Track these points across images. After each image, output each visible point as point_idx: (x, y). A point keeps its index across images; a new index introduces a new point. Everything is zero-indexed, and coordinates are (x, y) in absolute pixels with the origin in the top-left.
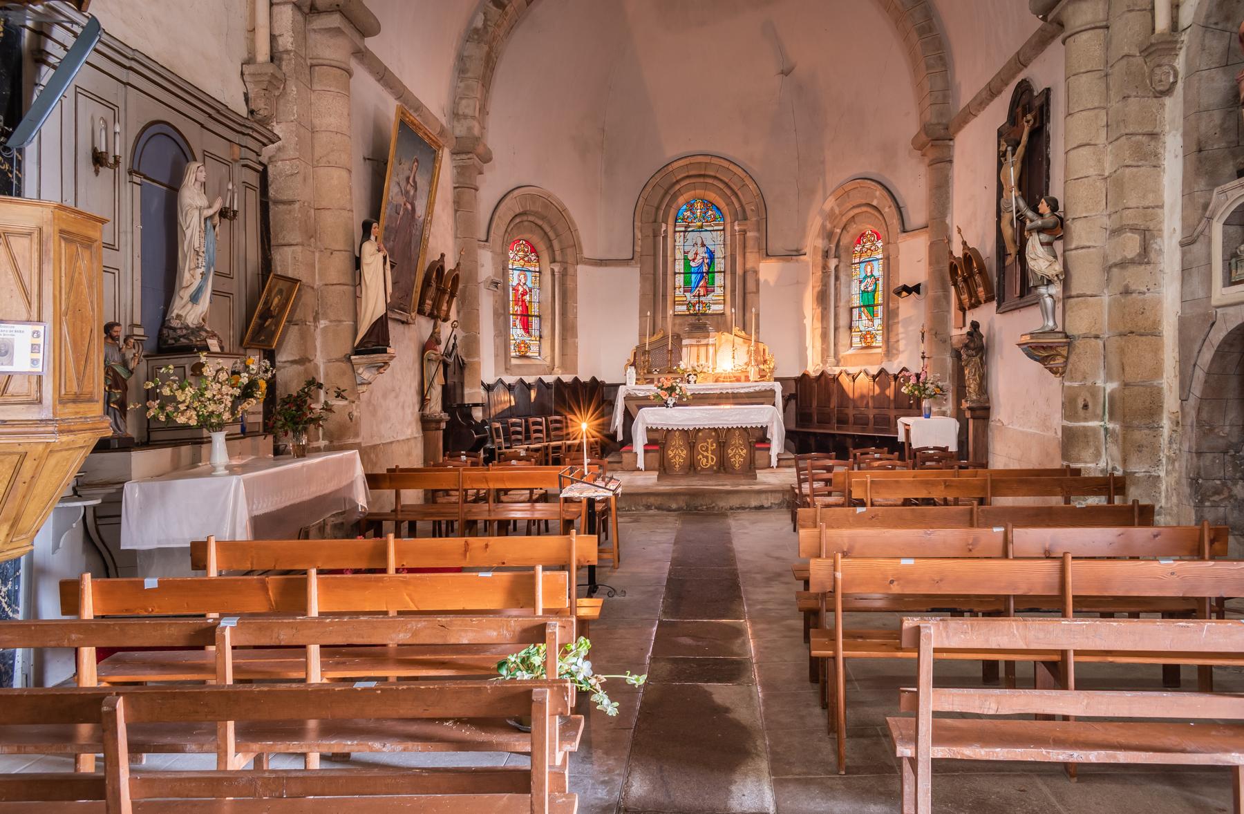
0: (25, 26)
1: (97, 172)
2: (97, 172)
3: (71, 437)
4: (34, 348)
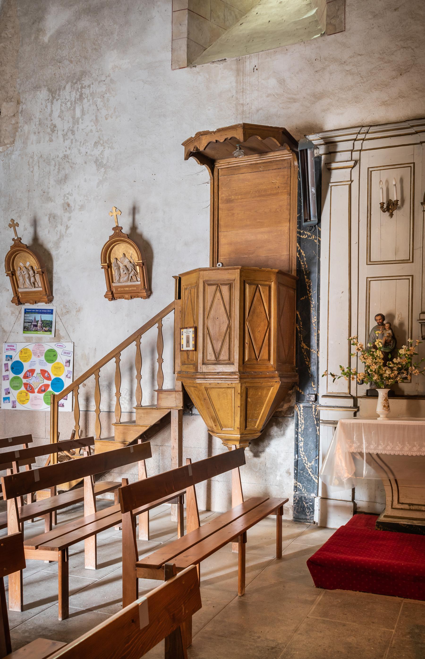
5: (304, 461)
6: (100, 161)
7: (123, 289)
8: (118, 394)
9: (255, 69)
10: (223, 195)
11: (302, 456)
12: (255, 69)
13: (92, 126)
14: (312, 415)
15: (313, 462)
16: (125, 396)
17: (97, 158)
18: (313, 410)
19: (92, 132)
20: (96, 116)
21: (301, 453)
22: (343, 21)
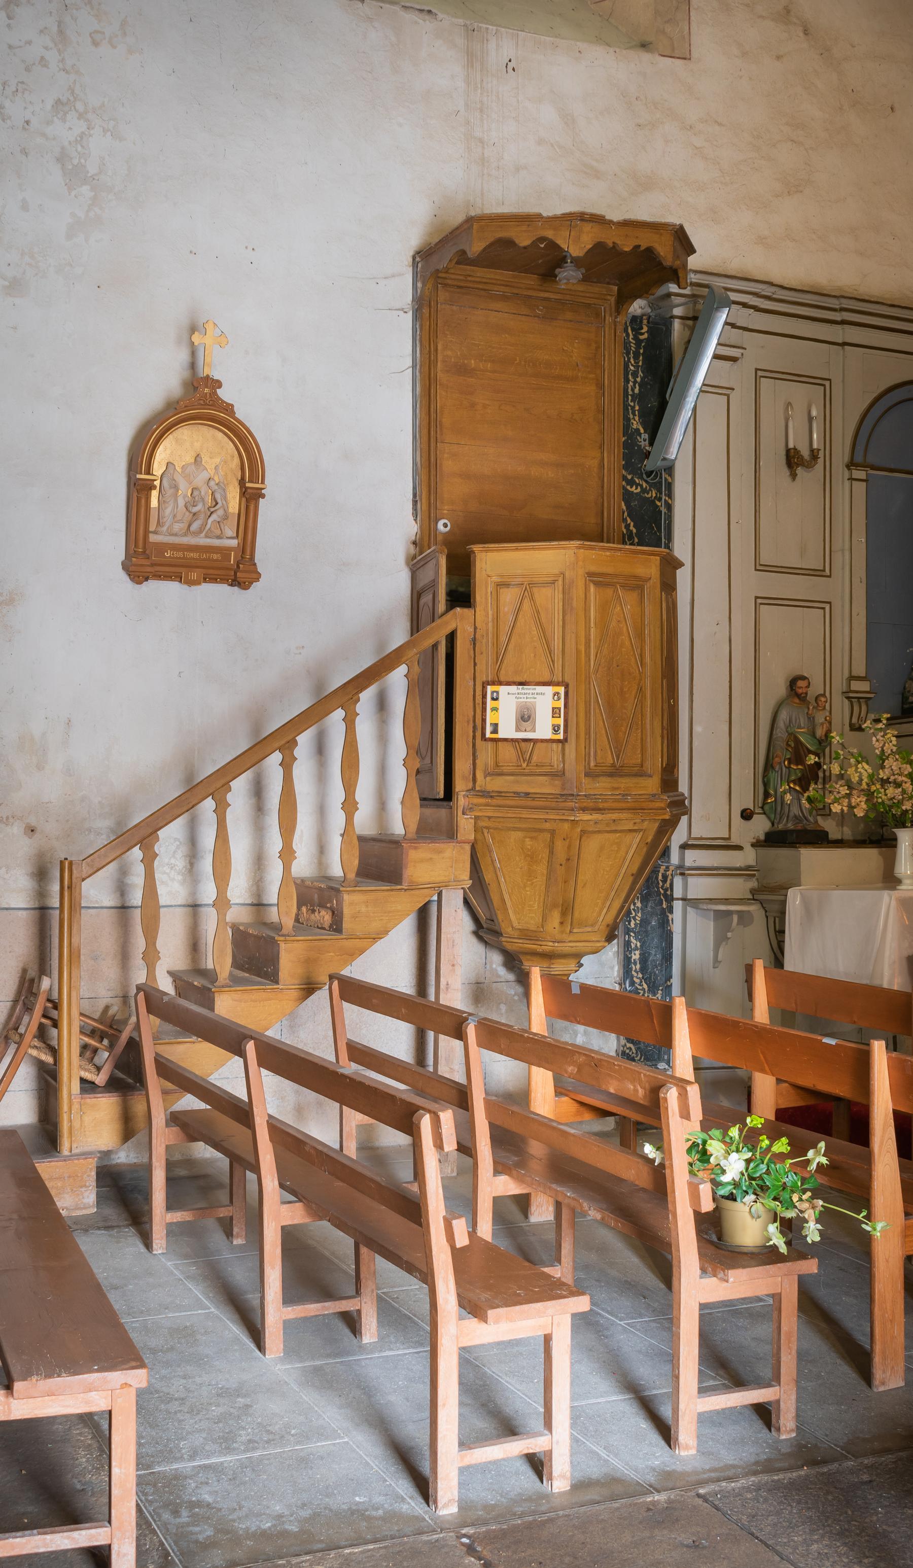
0: (673, 317)
1: (794, 476)
2: (794, 476)
3: (596, 816)
4: (555, 712)
5: (642, 992)
6: (75, 162)
7: (180, 554)
8: (259, 861)
9: (509, 66)
10: (449, 353)
11: (637, 981)
12: (509, 66)
13: (46, 48)
14: (658, 888)
15: (660, 992)
16: (173, 861)
17: (63, 148)
18: (660, 877)
19: (46, 66)
20: (60, 23)
21: (635, 974)
22: (687, 37)
